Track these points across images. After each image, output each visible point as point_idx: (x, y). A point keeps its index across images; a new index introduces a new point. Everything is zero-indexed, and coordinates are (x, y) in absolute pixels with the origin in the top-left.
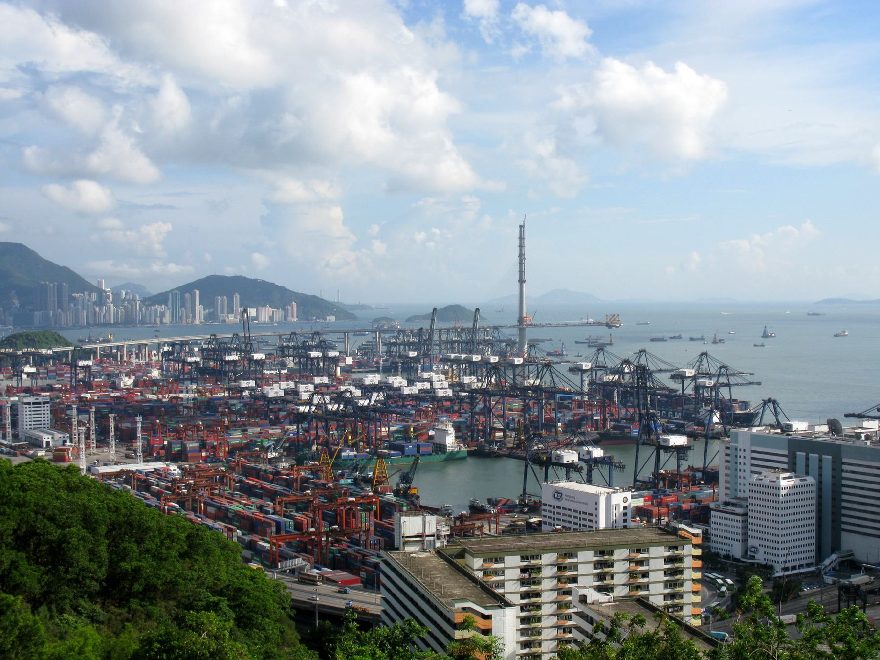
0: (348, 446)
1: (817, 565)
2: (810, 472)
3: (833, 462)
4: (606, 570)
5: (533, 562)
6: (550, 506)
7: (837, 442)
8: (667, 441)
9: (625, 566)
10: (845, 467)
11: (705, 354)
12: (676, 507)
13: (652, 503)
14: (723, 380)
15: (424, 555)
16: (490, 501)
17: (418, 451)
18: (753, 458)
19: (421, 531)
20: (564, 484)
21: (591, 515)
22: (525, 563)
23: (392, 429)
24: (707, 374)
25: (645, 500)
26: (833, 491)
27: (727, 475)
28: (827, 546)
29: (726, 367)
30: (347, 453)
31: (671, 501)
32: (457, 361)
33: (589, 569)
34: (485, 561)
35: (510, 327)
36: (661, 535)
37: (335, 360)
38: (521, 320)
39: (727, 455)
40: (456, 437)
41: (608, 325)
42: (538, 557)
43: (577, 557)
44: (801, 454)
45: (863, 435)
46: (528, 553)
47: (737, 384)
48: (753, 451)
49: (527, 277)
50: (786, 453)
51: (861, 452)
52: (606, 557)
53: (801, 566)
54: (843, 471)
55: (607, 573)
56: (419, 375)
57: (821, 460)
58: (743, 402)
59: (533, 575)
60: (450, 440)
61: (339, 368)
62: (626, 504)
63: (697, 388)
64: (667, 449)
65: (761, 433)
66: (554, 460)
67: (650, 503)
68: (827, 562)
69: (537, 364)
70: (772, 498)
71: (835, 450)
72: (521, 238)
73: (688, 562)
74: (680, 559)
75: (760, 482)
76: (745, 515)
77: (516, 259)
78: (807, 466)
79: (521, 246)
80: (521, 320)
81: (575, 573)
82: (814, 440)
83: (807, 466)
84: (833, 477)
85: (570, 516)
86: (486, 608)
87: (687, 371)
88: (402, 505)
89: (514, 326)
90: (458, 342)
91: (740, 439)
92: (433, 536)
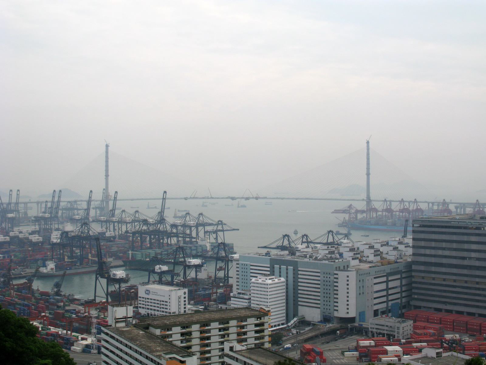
1: (286, 324)
2: (282, 275)
3: (294, 270)
6: (143, 298)
14: (220, 227)
19: (125, 315)
21: (167, 302)
28: (291, 314)
29: (221, 221)
33: (216, 332)
35: (227, 198)
39: (237, 267)
44: (277, 266)
45: (308, 256)
46: (185, 325)
50: (269, 266)
54: (299, 274)
57: (287, 269)
64: (190, 267)
68: (292, 322)
76: (250, 299)
78: (280, 272)
83: (280, 272)
85: (155, 303)
86: (182, 357)
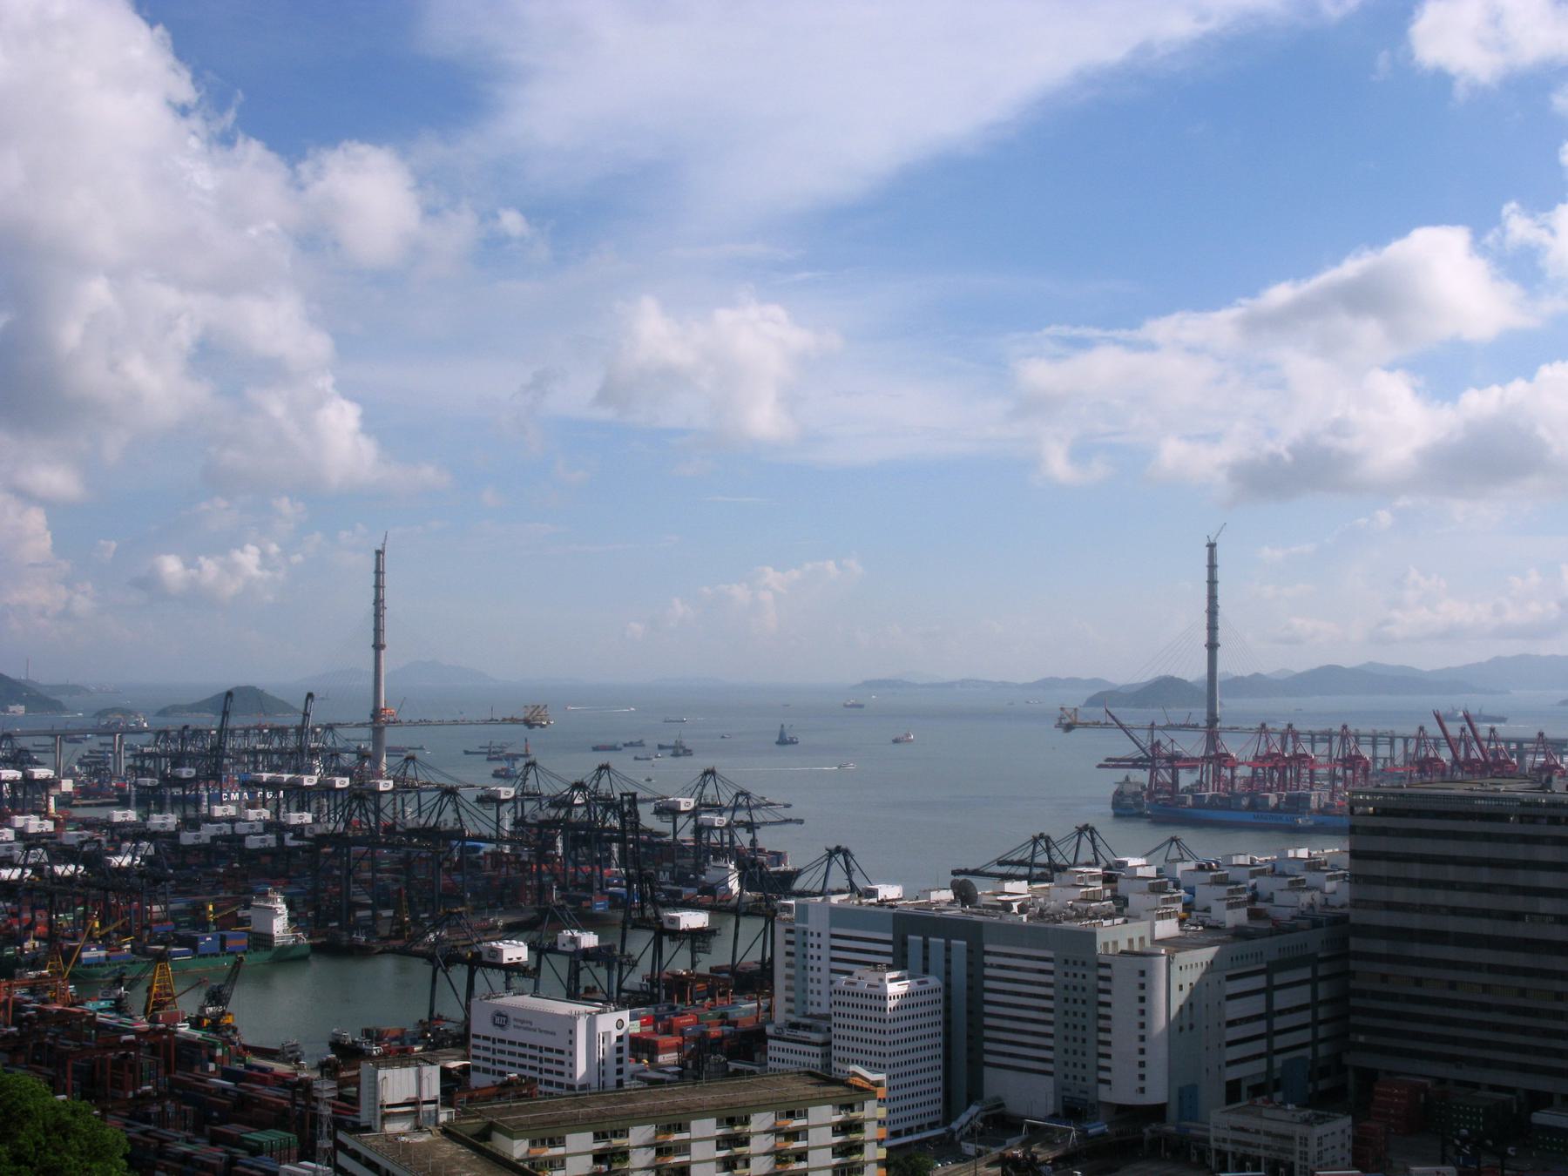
0: (95, 941)
3: (969, 951)
4: (738, 1150)
5: (616, 1142)
7: (976, 918)
8: (675, 920)
9: (768, 1143)
10: (988, 959)
11: (710, 772)
12: (697, 1034)
13: (655, 1028)
14: (742, 816)
15: (423, 1138)
16: (367, 1033)
17: (223, 947)
18: (833, 948)
19: (413, 1094)
20: (510, 1001)
21: (561, 1052)
22: (601, 1145)
23: (172, 907)
24: (715, 806)
25: (642, 1025)
26: (969, 1000)
27: (788, 977)
29: (747, 795)
30: (93, 953)
31: (688, 1025)
32: (273, 786)
34: (533, 1143)
35: (357, 726)
36: (818, 1085)
37: (46, 784)
38: (376, 713)
40: (291, 920)
41: (528, 723)
42: (624, 1133)
43: (688, 1129)
44: (915, 939)
46: (607, 1127)
47: (765, 823)
48: (834, 936)
49: (387, 638)
50: (889, 937)
51: (1015, 933)
52: (738, 1128)
53: (920, 1128)
54: (985, 965)
55: (738, 1156)
56: (205, 811)
57: (948, 949)
58: (774, 853)
59: (615, 1166)
60: (280, 926)
61: (52, 800)
62: (620, 1033)
63: (698, 830)
64: (677, 935)
65: (845, 905)
66: (485, 958)
67: (650, 1028)
68: (964, 1118)
69: (419, 790)
70: (873, 1014)
71: (972, 932)
72: (379, 572)
73: (871, 1131)
74: (857, 1126)
75: (851, 988)
77: (370, 608)
78: (926, 958)
79: (378, 586)
80: (376, 713)
81: (686, 1158)
82: (937, 915)
83: (926, 958)
84: (969, 976)
87: (682, 800)
88: (214, 1046)
89: (364, 725)
90: (265, 752)
91: (811, 917)
92: (435, 1102)
